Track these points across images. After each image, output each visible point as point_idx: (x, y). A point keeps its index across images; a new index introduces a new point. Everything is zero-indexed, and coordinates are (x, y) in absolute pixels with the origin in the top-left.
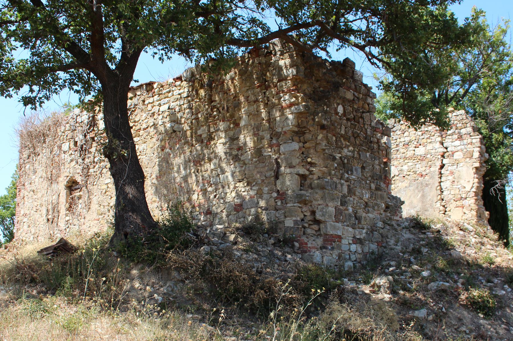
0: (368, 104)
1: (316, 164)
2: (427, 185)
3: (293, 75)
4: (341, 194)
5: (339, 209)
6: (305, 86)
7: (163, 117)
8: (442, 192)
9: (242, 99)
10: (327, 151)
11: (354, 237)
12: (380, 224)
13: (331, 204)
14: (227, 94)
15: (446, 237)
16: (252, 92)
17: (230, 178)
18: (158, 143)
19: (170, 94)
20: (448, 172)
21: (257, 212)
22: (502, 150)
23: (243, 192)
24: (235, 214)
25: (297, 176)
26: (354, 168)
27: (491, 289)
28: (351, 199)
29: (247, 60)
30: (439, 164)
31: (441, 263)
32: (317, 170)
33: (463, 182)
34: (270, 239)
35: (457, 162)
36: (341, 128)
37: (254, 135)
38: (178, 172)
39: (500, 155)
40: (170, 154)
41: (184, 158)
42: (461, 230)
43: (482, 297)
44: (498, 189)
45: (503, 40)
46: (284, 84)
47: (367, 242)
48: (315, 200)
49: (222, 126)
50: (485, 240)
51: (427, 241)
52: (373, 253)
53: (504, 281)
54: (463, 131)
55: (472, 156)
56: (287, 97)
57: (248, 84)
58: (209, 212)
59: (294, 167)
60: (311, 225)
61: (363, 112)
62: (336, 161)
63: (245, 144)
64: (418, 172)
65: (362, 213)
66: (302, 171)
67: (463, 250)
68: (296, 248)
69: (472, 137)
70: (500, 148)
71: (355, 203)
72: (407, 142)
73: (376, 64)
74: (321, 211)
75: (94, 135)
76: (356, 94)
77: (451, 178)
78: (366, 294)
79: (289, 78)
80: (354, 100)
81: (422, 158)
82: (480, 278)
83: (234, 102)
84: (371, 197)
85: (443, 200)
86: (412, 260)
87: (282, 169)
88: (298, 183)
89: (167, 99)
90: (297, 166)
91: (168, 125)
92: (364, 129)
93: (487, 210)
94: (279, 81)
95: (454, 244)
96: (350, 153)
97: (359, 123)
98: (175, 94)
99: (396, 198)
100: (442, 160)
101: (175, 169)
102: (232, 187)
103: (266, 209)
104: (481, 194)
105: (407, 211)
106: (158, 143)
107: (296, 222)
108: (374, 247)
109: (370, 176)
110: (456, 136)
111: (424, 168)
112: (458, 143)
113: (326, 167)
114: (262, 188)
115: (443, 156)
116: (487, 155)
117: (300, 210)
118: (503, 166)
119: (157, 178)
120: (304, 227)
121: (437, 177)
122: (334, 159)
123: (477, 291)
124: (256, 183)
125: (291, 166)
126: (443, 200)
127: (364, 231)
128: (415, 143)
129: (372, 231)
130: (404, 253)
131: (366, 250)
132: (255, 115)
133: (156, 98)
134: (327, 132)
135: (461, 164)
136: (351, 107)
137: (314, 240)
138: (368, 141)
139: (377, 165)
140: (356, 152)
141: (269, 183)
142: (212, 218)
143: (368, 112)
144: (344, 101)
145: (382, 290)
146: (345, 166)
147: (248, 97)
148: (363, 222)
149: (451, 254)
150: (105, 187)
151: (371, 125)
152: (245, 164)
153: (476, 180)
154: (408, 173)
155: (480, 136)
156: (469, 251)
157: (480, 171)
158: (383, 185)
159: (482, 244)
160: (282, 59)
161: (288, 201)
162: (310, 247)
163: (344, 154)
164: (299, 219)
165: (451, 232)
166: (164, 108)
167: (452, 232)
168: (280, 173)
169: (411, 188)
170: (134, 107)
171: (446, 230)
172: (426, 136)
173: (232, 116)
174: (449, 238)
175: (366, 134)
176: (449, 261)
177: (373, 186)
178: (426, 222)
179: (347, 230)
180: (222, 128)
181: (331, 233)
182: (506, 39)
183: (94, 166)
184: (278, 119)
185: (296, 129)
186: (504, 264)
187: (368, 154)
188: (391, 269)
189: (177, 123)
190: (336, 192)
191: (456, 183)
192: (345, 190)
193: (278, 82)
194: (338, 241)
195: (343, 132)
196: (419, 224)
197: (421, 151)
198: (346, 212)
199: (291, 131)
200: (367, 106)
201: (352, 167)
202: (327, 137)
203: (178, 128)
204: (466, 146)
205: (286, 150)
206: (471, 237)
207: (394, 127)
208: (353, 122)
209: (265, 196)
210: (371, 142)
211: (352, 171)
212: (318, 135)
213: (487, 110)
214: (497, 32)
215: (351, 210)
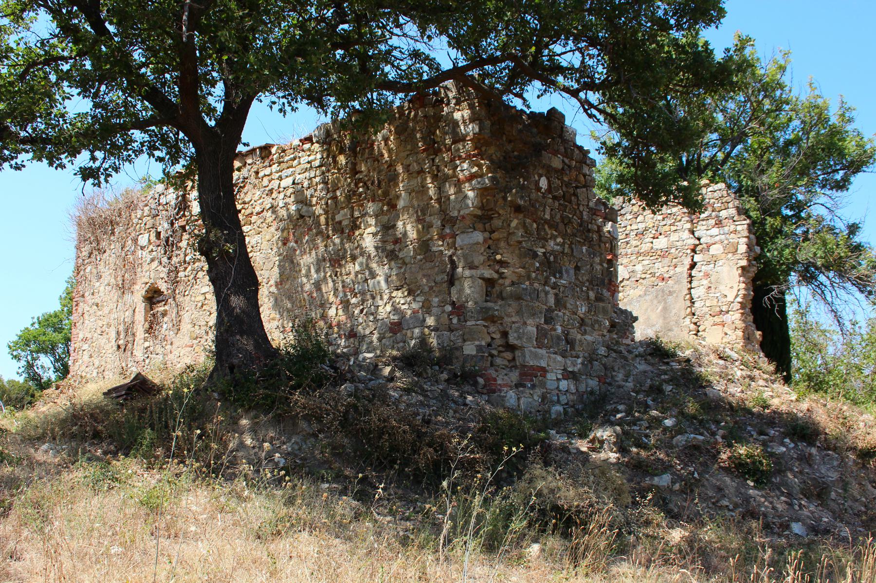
0: (585, 175)
2: (671, 293)
3: (474, 134)
6: (492, 150)
8: (693, 303)
9: (400, 169)
10: (524, 244)
11: (565, 370)
12: (602, 351)
14: (378, 161)
15: (699, 369)
16: (415, 158)
20: (702, 274)
21: (423, 333)
22: (780, 241)
25: (480, 281)
26: (564, 268)
27: (764, 444)
28: (560, 314)
30: (687, 262)
31: (691, 407)
33: (723, 289)
35: (714, 259)
37: (419, 220)
38: (308, 276)
42: (720, 358)
45: (781, 81)
47: (584, 377)
49: (371, 207)
50: (756, 373)
51: (670, 374)
52: (592, 393)
53: (783, 433)
54: (724, 214)
55: (737, 250)
57: (409, 147)
59: (476, 268)
61: (577, 187)
63: (405, 234)
64: (657, 275)
66: (488, 273)
68: (480, 387)
70: (777, 238)
75: (185, 223)
76: (567, 161)
77: (705, 282)
78: (582, 452)
79: (468, 138)
80: (563, 169)
81: (664, 254)
82: (749, 428)
84: (589, 311)
85: (694, 314)
86: (650, 402)
87: (460, 270)
89: (291, 169)
90: (481, 267)
91: (293, 208)
95: (711, 378)
99: (625, 312)
100: (693, 256)
102: (386, 297)
104: (749, 306)
105: (641, 332)
107: (479, 348)
108: (593, 383)
109: (587, 280)
110: (712, 222)
111: (666, 269)
112: (715, 231)
113: (524, 268)
116: (758, 249)
120: (492, 356)
122: (535, 255)
125: (472, 267)
126: (694, 314)
127: (580, 361)
128: (654, 232)
130: (637, 393)
131: (582, 388)
133: (275, 167)
134: (524, 217)
140: (567, 246)
141: (439, 291)
143: (585, 186)
144: (549, 171)
145: (605, 446)
146: (551, 266)
147: (409, 165)
148: (577, 348)
149: (706, 394)
150: (202, 298)
151: (588, 205)
152: (404, 263)
153: (743, 286)
155: (748, 221)
157: (748, 272)
158: (606, 293)
159: (752, 379)
160: (459, 110)
163: (549, 248)
164: (483, 343)
168: (456, 277)
170: (243, 182)
173: (386, 194)
174: (703, 370)
177: (592, 295)
178: (670, 346)
180: (370, 211)
181: (531, 364)
182: (786, 79)
183: (186, 268)
184: (452, 197)
185: (479, 213)
186: (784, 408)
187: (584, 248)
188: (619, 416)
189: (306, 205)
190: (537, 304)
191: (713, 290)
192: (552, 300)
195: (547, 216)
196: (660, 350)
197: (661, 243)
198: (553, 333)
200: (582, 178)
202: (525, 223)
206: (736, 369)
207: (622, 208)
210: (589, 231)
211: (561, 273)
212: (511, 221)
213: (758, 183)
214: (772, 69)
215: (559, 329)
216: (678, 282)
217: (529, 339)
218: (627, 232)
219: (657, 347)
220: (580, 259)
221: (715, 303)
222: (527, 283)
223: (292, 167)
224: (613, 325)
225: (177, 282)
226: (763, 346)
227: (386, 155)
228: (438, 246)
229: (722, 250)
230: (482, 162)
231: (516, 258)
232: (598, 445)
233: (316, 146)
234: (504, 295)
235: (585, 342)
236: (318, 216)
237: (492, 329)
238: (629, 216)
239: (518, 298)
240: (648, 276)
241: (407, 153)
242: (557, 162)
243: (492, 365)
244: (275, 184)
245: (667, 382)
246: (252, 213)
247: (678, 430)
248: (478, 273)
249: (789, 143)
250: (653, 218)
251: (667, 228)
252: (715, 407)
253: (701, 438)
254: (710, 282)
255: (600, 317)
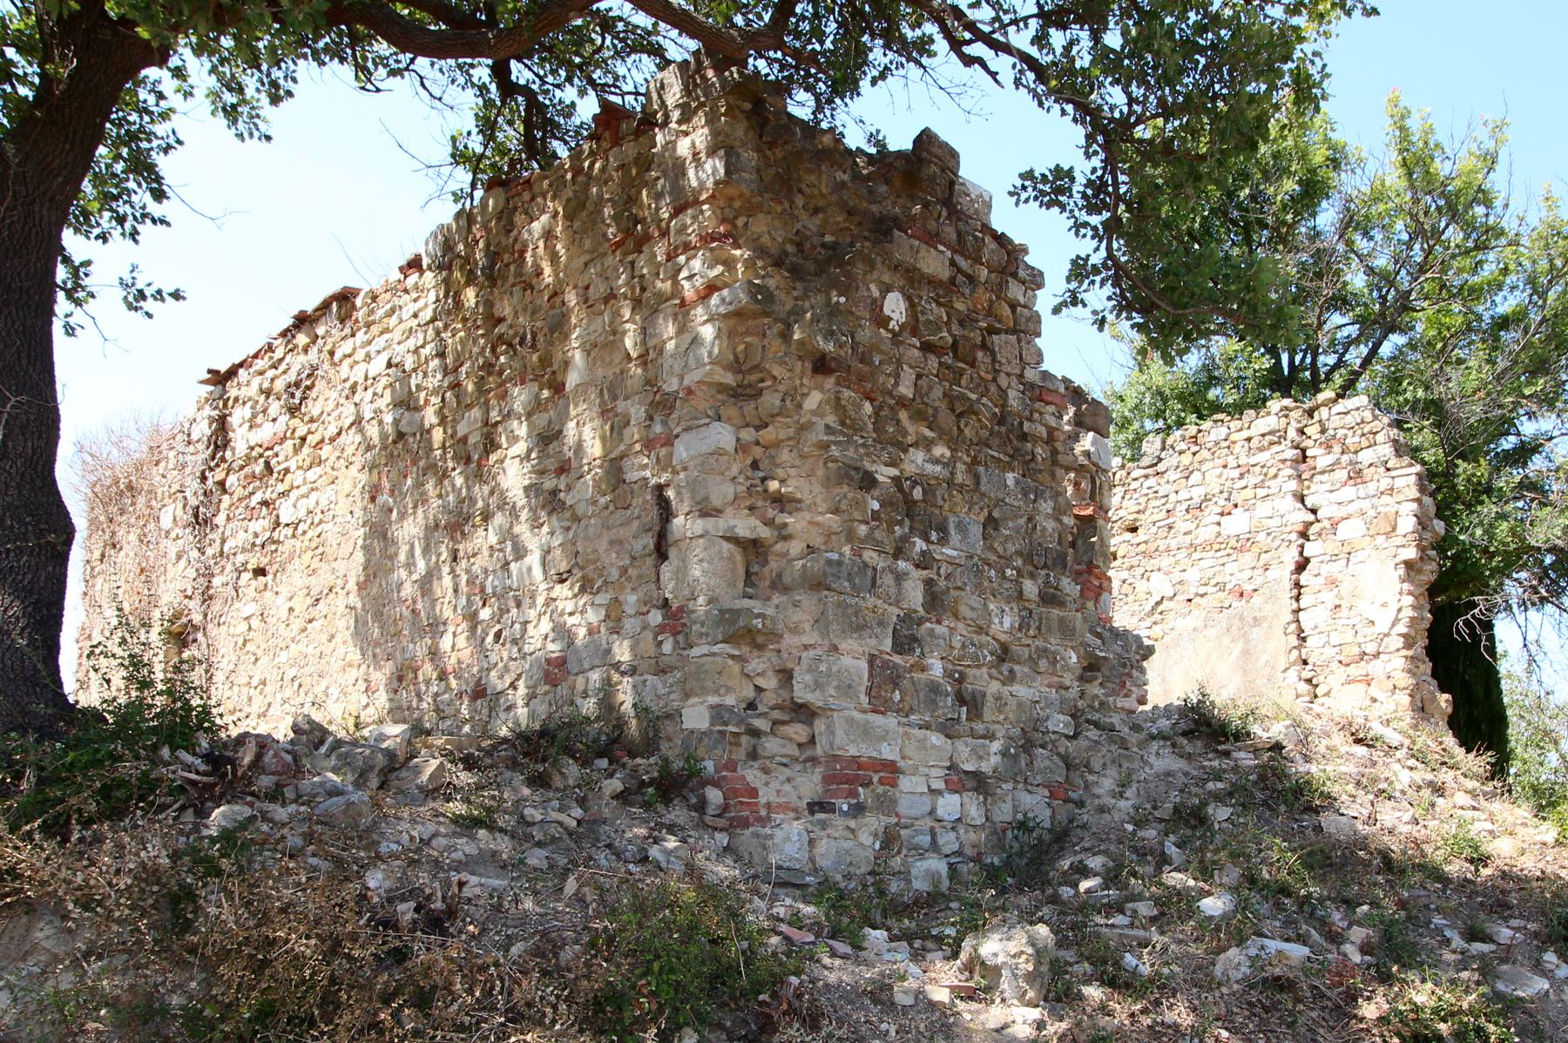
0: (1013, 306)
1: (800, 501)
2: (1256, 621)
3: (717, 183)
4: (897, 611)
5: (886, 665)
6: (760, 225)
7: (375, 394)
8: (1304, 639)
9: (572, 298)
10: (835, 451)
11: (952, 767)
12: (1059, 723)
13: (849, 644)
14: (532, 288)
15: (1303, 768)
16: (599, 266)
17: (537, 572)
18: (364, 478)
19: (394, 320)
20: (1321, 580)
21: (607, 681)
22: (1489, 509)
23: (571, 614)
24: (546, 693)
25: (726, 546)
26: (952, 520)
27: (1487, 972)
28: (940, 630)
29: (586, 164)
30: (1291, 557)
31: (1279, 856)
32: (803, 524)
33: (1367, 609)
34: (611, 776)
35: (1347, 549)
36: (897, 376)
37: (605, 413)
38: (410, 565)
39: (1481, 523)
40: (391, 511)
41: (426, 518)
42: (1358, 741)
43: (1452, 1014)
44: (1479, 621)
45: (1487, 186)
46: (689, 222)
47: (1007, 786)
48: (790, 630)
49: (520, 397)
50: (1446, 776)
51: (1236, 780)
52: (1023, 826)
53: (1536, 935)
54: (1366, 457)
55: (1394, 528)
56: (697, 264)
57: (588, 243)
58: (479, 692)
59: (716, 512)
60: (784, 723)
61: (991, 331)
62: (876, 493)
63: (579, 447)
64: (1228, 587)
65: (984, 681)
66: (746, 526)
67: (1365, 812)
68: (711, 810)
69: (1393, 473)
70: (1481, 503)
71: (957, 644)
72: (1196, 501)
73: (981, 62)
74: (810, 670)
75: (223, 475)
76: (963, 263)
77: (1329, 598)
78: (933, 1005)
79: (704, 197)
80: (952, 281)
81: (1243, 544)
82: (1438, 920)
83: (552, 312)
84: (1023, 626)
85: (1305, 663)
86: (1172, 850)
87: (678, 521)
88: (733, 570)
89: (386, 336)
90: (729, 511)
91: (388, 418)
92: (993, 388)
93: (1443, 689)
94: (677, 211)
95: (1335, 789)
96: (938, 468)
97: (972, 365)
98: (405, 317)
99: (1122, 636)
100: (1302, 546)
101: (402, 557)
102: (540, 600)
103: (633, 671)
104: (1423, 642)
105: (1167, 684)
106: (364, 478)
107: (718, 713)
108: (1035, 804)
109: (1019, 553)
110: (1341, 475)
111: (1249, 573)
112: (1349, 492)
113: (836, 511)
114: (621, 598)
115: (1304, 535)
116: (1440, 526)
117: (735, 668)
118: (1493, 555)
119: (361, 587)
120: (755, 733)
121: (1286, 591)
122: (868, 482)
123: (1429, 985)
124: (606, 582)
125: (706, 511)
126: (1305, 663)
127: (996, 746)
128: (1222, 502)
129: (1028, 746)
130: (1139, 824)
131: (1003, 813)
132: (604, 346)
133: (361, 336)
134: (838, 383)
135: (1360, 556)
136: (939, 304)
137: (789, 780)
138: (1010, 431)
139: (1048, 516)
140: (960, 467)
141: (640, 577)
142: (485, 711)
143: (1014, 331)
144: (912, 281)
145: (1005, 984)
146: (913, 510)
147: (587, 288)
148: (988, 714)
149: (1318, 829)
150: (243, 627)
151: (1021, 376)
152: (576, 519)
153: (1410, 600)
154: (1202, 590)
155: (1418, 468)
156: (1388, 815)
157: (1419, 571)
158: (1069, 587)
159: (1439, 790)
160: (686, 134)
161: (693, 638)
162: (768, 805)
163: (910, 469)
164: (730, 700)
165: (1322, 749)
166: (378, 365)
167: (1327, 748)
168: (671, 538)
169: (1210, 632)
170: (309, 376)
171: (1304, 741)
172: (1251, 480)
173: (545, 361)
174: (1314, 769)
175: (1004, 406)
176: (1310, 854)
177: (1030, 588)
178: (1234, 717)
179: (922, 743)
180: (518, 406)
181: (853, 751)
182: (1497, 182)
183: (223, 568)
184: (671, 345)
185: (729, 379)
186: (1529, 865)
187: (1010, 478)
188: (1085, 885)
189: (408, 409)
190: (871, 601)
191: (1344, 612)
192: (915, 595)
193: (670, 220)
194: (881, 782)
195: (905, 389)
196: (1209, 725)
197: (1237, 524)
198: (917, 675)
199: (710, 384)
200: (1006, 311)
201: (946, 519)
202: (838, 399)
203: (409, 423)
204: (1375, 500)
205: (693, 453)
206: (1397, 767)
207: (1160, 460)
208: (948, 359)
209: (630, 625)
210: (1024, 437)
211: (943, 529)
212: (804, 395)
213: (1439, 390)
214: (1466, 162)
215: (937, 669)
216: (1271, 598)
217: (847, 689)
218: (1169, 506)
219: (1200, 715)
220: (999, 502)
221: (1348, 636)
222: (847, 550)
223: (386, 330)
224: (1091, 667)
225: (211, 598)
226: (1454, 723)
227: (547, 271)
228: (642, 469)
229: (1362, 529)
230: (738, 252)
231: (818, 488)
232: (982, 983)
233: (429, 275)
234: (787, 579)
235: (1012, 702)
236: (429, 431)
237: (755, 664)
238: (1172, 476)
239: (818, 585)
240: (1210, 589)
241: (586, 257)
242: (934, 262)
243: (753, 755)
244: (358, 375)
245: (1218, 797)
246: (322, 441)
247: (1233, 931)
248: (720, 524)
249: (1504, 323)
250: (1220, 476)
251: (1249, 493)
252: (1347, 865)
253: (1298, 951)
254: (1338, 596)
255: (1054, 643)
